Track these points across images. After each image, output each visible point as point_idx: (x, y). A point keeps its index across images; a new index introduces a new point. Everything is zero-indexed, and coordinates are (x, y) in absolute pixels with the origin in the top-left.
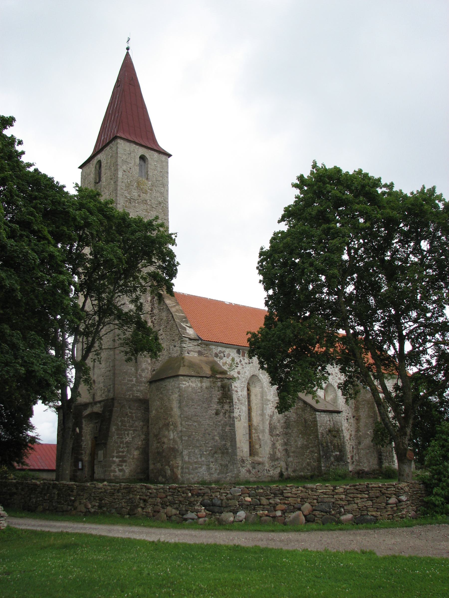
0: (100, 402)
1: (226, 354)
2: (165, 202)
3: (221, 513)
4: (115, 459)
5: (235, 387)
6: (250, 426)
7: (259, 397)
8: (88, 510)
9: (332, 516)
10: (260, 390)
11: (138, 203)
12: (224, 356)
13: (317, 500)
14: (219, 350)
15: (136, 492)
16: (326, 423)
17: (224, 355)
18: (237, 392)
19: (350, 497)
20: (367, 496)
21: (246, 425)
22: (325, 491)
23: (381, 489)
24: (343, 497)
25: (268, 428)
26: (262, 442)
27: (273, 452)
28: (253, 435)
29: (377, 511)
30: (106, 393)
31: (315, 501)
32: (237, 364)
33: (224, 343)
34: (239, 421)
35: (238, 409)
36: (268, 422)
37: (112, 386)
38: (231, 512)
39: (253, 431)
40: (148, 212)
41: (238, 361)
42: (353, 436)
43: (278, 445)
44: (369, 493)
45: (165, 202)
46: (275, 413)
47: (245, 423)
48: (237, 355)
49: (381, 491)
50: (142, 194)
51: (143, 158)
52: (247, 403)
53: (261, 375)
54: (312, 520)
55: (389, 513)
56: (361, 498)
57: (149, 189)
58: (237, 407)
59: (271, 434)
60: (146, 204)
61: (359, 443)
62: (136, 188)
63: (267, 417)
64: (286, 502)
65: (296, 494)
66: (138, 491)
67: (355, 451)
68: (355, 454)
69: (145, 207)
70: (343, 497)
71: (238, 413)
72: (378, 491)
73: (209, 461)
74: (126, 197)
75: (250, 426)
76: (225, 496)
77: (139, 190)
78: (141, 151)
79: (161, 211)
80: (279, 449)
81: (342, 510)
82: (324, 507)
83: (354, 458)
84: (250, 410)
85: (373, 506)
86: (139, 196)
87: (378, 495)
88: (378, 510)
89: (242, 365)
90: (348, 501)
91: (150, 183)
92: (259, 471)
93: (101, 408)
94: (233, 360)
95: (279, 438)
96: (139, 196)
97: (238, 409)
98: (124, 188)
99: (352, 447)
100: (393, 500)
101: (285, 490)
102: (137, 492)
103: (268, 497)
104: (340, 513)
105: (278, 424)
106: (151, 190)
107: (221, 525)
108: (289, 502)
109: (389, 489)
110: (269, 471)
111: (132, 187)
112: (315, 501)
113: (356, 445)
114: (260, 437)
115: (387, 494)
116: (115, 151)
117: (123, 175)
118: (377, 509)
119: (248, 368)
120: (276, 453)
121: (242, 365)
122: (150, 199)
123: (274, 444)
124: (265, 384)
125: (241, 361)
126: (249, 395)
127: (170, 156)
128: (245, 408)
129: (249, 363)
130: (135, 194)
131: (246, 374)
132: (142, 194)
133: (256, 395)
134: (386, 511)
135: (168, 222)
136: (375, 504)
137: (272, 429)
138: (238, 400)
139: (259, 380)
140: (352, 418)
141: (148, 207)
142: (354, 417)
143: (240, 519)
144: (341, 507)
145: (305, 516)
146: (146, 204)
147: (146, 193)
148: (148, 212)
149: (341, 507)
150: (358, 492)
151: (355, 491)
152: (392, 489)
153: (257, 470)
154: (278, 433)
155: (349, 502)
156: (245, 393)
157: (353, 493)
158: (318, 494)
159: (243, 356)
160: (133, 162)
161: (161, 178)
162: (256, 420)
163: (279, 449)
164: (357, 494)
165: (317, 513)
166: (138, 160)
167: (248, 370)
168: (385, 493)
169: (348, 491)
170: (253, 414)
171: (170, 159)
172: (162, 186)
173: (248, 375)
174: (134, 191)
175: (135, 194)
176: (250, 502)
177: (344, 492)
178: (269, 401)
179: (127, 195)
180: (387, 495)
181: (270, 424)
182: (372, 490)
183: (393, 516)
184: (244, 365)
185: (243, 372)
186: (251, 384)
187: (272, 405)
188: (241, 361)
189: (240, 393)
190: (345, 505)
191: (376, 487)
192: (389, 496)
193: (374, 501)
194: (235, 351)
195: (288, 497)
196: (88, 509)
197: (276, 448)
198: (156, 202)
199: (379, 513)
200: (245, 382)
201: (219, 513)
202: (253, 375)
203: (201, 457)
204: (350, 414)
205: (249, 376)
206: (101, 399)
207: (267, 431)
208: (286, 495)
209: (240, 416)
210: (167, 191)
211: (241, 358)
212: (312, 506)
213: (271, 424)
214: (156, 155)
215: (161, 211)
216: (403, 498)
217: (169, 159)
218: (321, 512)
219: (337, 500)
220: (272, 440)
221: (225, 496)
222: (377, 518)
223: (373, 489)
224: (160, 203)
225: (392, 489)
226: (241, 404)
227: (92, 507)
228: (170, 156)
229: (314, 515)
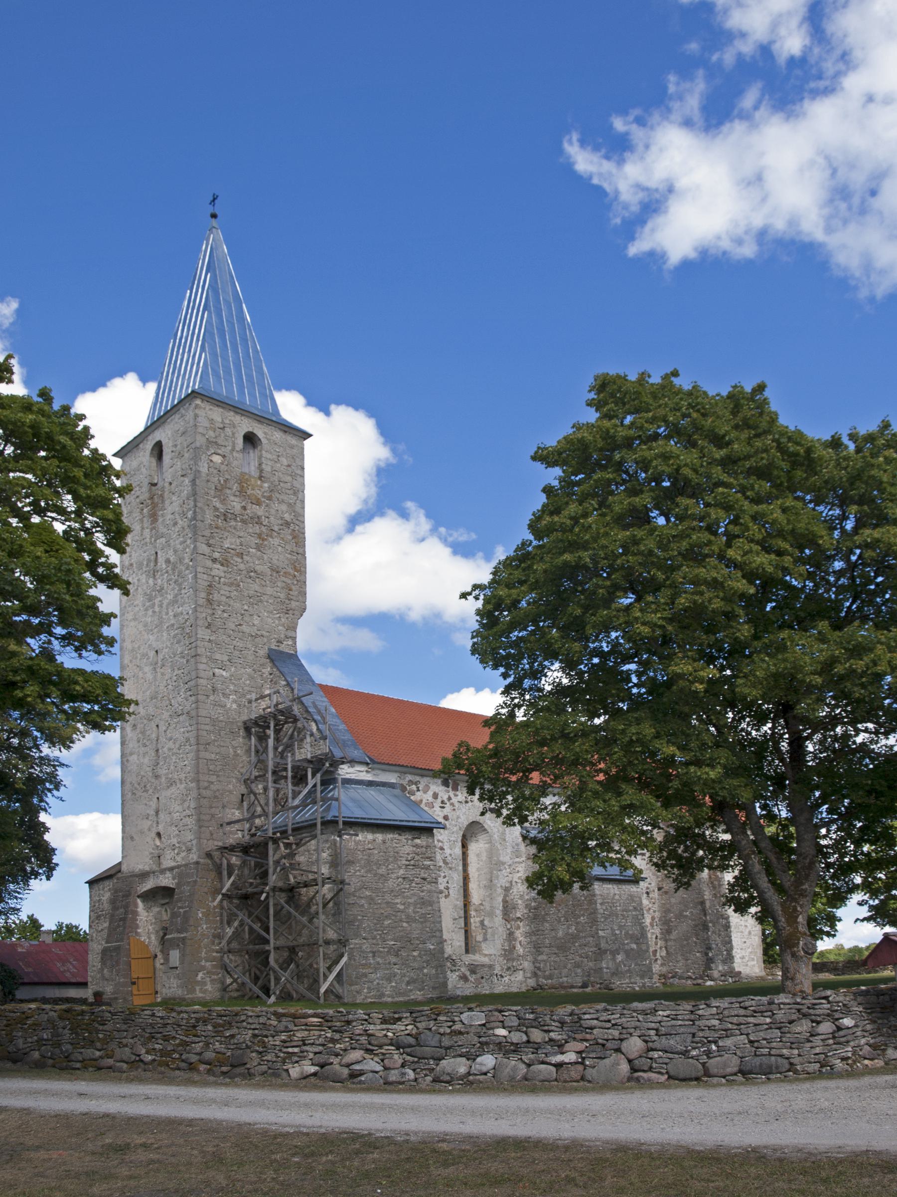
0: (171, 869)
1: (421, 787)
2: (297, 522)
3: (440, 1060)
4: (203, 963)
5: (439, 841)
6: (466, 905)
7: (484, 858)
8: (137, 1058)
9: (690, 1060)
10: (487, 845)
11: (243, 521)
12: (418, 790)
13: (657, 1030)
14: (407, 779)
15: (245, 1024)
16: (613, 898)
17: (418, 788)
18: (442, 849)
19: (731, 1023)
20: (768, 1020)
21: (460, 904)
22: (673, 1013)
23: (801, 1007)
24: (716, 1022)
25: (501, 908)
26: (490, 931)
27: (510, 946)
28: (472, 920)
29: (791, 1048)
30: (183, 854)
31: (653, 1032)
32: (443, 802)
33: (417, 768)
34: (446, 897)
35: (445, 877)
36: (500, 899)
37: (194, 842)
38: (461, 1056)
39: (473, 913)
40: (263, 540)
41: (445, 798)
42: (657, 920)
43: (519, 935)
44: (773, 1014)
45: (297, 522)
46: (514, 884)
47: (457, 900)
48: (444, 788)
49: (799, 1010)
50: (249, 506)
51: (250, 439)
52: (461, 868)
53: (489, 822)
54: (646, 1069)
55: (817, 1050)
56: (756, 1025)
57: (264, 497)
58: (443, 875)
59: (506, 917)
60: (259, 523)
61: (669, 932)
62: (238, 493)
63: (499, 890)
64: (588, 1037)
65: (609, 1021)
66: (250, 1020)
67: (660, 942)
68: (661, 948)
69: (257, 528)
70: (716, 1022)
71: (444, 885)
72: (793, 1011)
73: (389, 963)
74: (216, 509)
75: (465, 905)
76: (450, 1027)
77: (243, 498)
78: (245, 425)
79: (290, 537)
80: (520, 942)
81: (714, 1047)
82: (672, 1042)
83: (658, 954)
84: (466, 879)
85: (784, 1039)
86: (244, 508)
87: (794, 1017)
88: (793, 1046)
89: (452, 804)
90: (725, 1030)
91: (266, 485)
92: (482, 978)
93: (174, 879)
94: (435, 796)
95: (521, 924)
96: (244, 508)
97: (445, 877)
98: (212, 492)
99: (654, 936)
100: (826, 1027)
101: (585, 1014)
102: (248, 1023)
103: (546, 1028)
104: (708, 1053)
105: (520, 902)
106: (270, 498)
107: (443, 1083)
108: (593, 1037)
109: (816, 1007)
110: (502, 976)
111: (228, 491)
112: (653, 1032)
113: (662, 933)
114: (486, 923)
115: (815, 1015)
116: (192, 423)
117: (209, 467)
118: (792, 1043)
119: (464, 810)
120: (514, 948)
121: (452, 804)
122: (267, 514)
123: (511, 935)
124: (496, 836)
125: (449, 799)
126: (465, 855)
127: (306, 435)
128: (456, 878)
129: (467, 802)
130: (236, 505)
131: (460, 820)
132: (249, 506)
133: (478, 855)
134: (812, 1048)
135: (305, 558)
136: (788, 1035)
137: (508, 908)
138: (445, 862)
139: (485, 830)
140: (656, 890)
141: (264, 529)
142: (659, 889)
143: (484, 1069)
144: (709, 1042)
145: (630, 1061)
146: (259, 523)
147: (258, 503)
148: (263, 540)
149: (709, 1042)
150: (748, 1012)
151: (742, 1012)
152: (825, 1006)
153: (479, 976)
154: (518, 915)
155: (728, 1033)
156: (458, 850)
157: (737, 1016)
158: (659, 1018)
159: (455, 788)
160: (231, 444)
161: (289, 478)
162: (476, 895)
163: (520, 942)
164: (747, 1016)
165: (655, 1055)
166: (240, 441)
167: (465, 814)
168: (810, 1015)
169: (726, 1013)
170: (473, 886)
171: (307, 443)
172: (291, 492)
173: (464, 821)
174: (232, 498)
175: (236, 505)
176: (505, 1037)
177: (718, 1014)
178: (503, 863)
179: (218, 505)
180: (813, 1017)
181: (505, 901)
182: (780, 1009)
183: (827, 1056)
184: (457, 805)
185: (455, 817)
186: (468, 837)
187: (508, 870)
188: (449, 799)
189: (448, 851)
190: (720, 1038)
191: (789, 1004)
192: (819, 1019)
193: (784, 1030)
194: (439, 781)
195: (592, 1028)
196: (139, 1056)
197: (515, 940)
198: (280, 522)
199: (796, 1052)
200: (457, 833)
201: (434, 1059)
202: (473, 822)
203: (374, 956)
204: (653, 885)
205: (466, 823)
206: (173, 864)
207: (499, 912)
208: (586, 1024)
209: (447, 888)
210: (303, 502)
211: (451, 794)
212: (646, 1042)
213: (507, 902)
214: (278, 435)
215: (290, 537)
216: (847, 1022)
217: (306, 442)
218: (666, 1052)
219: (703, 1030)
220: (509, 926)
221: (450, 1027)
222: (792, 1060)
223: (782, 1006)
224: (287, 524)
225: (825, 1006)
226: (451, 869)
227: (147, 1053)
228: (306, 435)
229: (651, 1059)
